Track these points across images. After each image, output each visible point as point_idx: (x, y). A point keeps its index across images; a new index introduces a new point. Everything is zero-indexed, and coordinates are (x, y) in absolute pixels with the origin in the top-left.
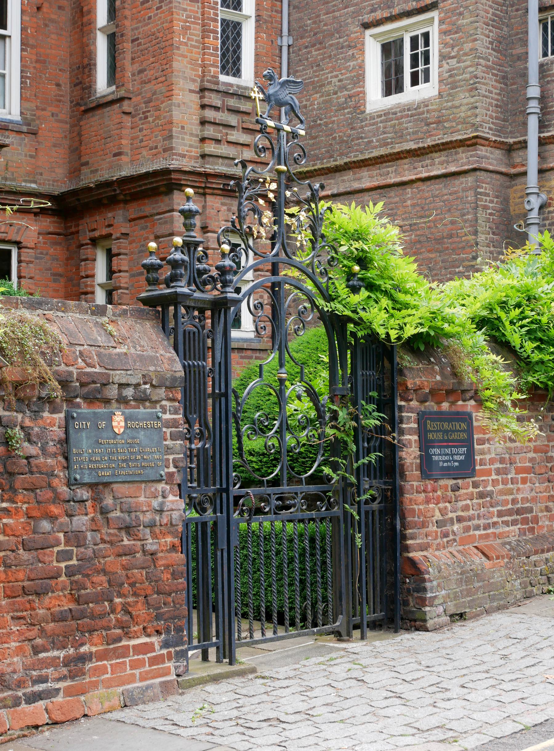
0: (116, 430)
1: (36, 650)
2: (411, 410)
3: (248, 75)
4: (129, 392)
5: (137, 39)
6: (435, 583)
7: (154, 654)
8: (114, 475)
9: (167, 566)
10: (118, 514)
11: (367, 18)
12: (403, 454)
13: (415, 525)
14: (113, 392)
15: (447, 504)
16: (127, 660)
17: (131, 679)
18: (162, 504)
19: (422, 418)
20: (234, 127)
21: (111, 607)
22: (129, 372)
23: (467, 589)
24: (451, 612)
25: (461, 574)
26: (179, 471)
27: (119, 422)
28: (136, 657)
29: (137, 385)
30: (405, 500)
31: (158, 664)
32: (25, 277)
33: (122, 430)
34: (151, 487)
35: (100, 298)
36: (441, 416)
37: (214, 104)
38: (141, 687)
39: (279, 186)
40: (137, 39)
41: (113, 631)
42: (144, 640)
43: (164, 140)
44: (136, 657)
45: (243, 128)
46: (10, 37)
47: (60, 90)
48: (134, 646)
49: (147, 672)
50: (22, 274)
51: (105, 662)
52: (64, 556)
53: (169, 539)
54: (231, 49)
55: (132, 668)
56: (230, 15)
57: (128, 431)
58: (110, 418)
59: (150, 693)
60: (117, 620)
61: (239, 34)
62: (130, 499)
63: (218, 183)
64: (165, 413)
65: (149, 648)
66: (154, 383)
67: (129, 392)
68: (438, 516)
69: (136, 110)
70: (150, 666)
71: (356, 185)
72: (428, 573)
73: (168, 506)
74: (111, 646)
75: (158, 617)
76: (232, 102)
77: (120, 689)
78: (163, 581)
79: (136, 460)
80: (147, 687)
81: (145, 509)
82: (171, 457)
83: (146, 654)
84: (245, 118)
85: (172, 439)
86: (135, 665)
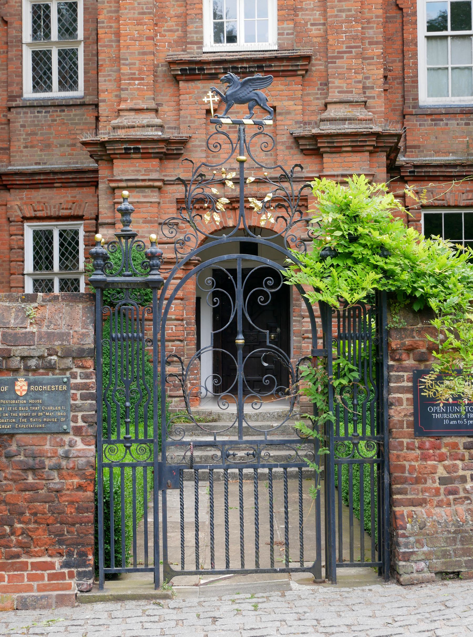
0: (18, 393)
2: (405, 369)
4: (33, 363)
6: (412, 539)
7: (54, 571)
8: (13, 428)
9: (71, 503)
10: (22, 458)
12: (392, 412)
13: (405, 481)
14: (15, 363)
15: (458, 462)
16: (25, 573)
17: (30, 588)
18: (67, 452)
21: (11, 530)
22: (32, 347)
23: (463, 549)
24: (438, 570)
25: (455, 532)
26: (90, 426)
27: (21, 386)
28: (34, 572)
29: (41, 357)
30: (391, 456)
31: (57, 580)
33: (24, 393)
34: (56, 438)
35: (29, 288)
38: (37, 597)
41: (13, 549)
42: (46, 559)
44: (34, 572)
48: (32, 563)
49: (45, 585)
51: (3, 573)
53: (76, 481)
55: (29, 580)
57: (31, 394)
58: (13, 383)
59: (44, 602)
60: (17, 541)
62: (34, 447)
64: (75, 378)
65: (51, 566)
66: (59, 354)
67: (33, 363)
68: (441, 472)
70: (48, 580)
72: (405, 528)
73: (73, 453)
74: (10, 561)
75: (60, 542)
77: (15, 596)
78: (67, 514)
79: (37, 416)
80: (42, 598)
81: (49, 455)
82: (80, 414)
83: (45, 570)
85: (82, 399)
86: (32, 578)
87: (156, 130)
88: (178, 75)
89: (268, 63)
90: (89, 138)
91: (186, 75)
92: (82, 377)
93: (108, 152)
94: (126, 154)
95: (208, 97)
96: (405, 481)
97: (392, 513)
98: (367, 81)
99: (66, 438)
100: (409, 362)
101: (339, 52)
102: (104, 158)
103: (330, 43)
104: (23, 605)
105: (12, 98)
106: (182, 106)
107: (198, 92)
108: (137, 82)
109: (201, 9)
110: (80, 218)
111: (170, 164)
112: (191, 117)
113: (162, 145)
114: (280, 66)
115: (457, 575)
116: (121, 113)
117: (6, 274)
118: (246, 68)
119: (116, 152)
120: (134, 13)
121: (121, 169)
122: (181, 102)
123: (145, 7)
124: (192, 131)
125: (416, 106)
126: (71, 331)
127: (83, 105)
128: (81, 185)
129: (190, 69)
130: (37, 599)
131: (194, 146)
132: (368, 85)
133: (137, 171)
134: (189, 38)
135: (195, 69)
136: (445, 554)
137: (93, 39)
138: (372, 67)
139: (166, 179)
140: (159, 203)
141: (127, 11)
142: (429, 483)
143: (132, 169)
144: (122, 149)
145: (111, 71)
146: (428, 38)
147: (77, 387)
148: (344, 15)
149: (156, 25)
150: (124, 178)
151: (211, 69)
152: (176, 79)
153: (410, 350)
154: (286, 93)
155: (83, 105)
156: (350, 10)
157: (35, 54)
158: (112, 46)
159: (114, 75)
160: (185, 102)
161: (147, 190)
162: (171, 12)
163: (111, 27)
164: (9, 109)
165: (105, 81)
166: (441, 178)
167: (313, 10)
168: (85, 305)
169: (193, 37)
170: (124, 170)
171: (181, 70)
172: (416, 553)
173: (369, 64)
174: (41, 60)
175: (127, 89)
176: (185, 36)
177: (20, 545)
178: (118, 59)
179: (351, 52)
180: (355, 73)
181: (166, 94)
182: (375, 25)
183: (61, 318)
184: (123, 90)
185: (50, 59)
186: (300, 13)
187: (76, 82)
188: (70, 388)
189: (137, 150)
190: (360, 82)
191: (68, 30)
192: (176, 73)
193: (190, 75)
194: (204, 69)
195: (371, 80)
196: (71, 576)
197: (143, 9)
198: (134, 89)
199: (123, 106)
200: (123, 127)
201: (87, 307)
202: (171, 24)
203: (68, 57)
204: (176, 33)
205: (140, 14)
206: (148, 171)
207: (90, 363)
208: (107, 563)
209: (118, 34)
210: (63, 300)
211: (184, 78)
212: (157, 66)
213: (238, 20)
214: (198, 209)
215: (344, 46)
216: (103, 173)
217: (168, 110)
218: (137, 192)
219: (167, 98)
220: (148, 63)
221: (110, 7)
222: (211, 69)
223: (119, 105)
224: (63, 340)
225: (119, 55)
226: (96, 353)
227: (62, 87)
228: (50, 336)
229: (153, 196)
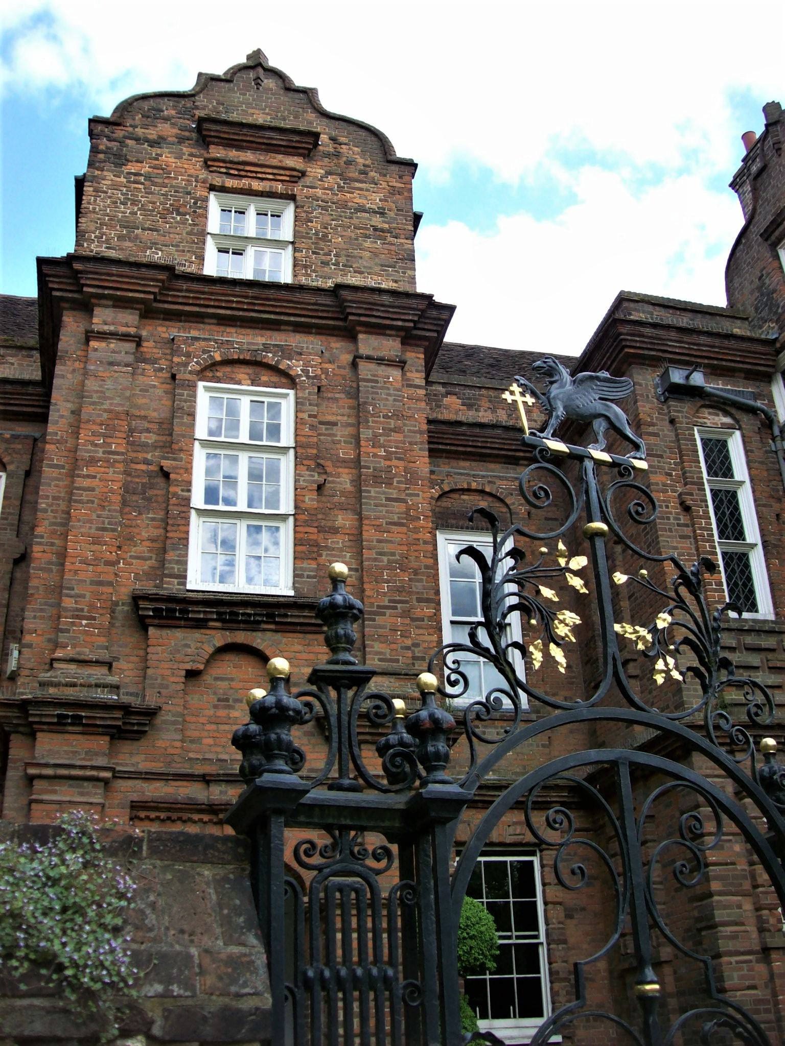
3: (765, 609)
5: (633, 594)
20: (757, 668)
32: (550, 884)
37: (728, 645)
39: (593, 560)
40: (633, 594)
43: (674, 696)
45: (769, 668)
46: (510, 624)
47: (573, 672)
50: (547, 881)
54: (740, 584)
56: (733, 546)
61: (747, 566)
69: (643, 671)
76: (749, 640)
84: (770, 656)
87: (110, 692)
88: (149, 616)
89: (282, 611)
91: (161, 617)
93: (31, 719)
94: (60, 725)
95: (512, 393)
98: (416, 650)
101: (379, 607)
102: (21, 729)
103: (367, 593)
106: (150, 663)
107: (176, 645)
108: (84, 622)
109: (187, 532)
112: (163, 678)
113: (118, 714)
114: (299, 616)
116: (56, 665)
118: (249, 615)
119: (44, 720)
120: (90, 528)
121: (47, 747)
122: (149, 657)
123: (107, 521)
124: (163, 700)
126: (194, 951)
129: (167, 610)
131: (165, 722)
132: (417, 654)
133: (75, 753)
134: (168, 568)
135: (175, 610)
138: (421, 631)
139: (118, 768)
140: (103, 806)
141: (81, 524)
143: (66, 748)
144: (53, 716)
145: (46, 604)
146: (452, 622)
148: (385, 559)
149: (119, 548)
150: (52, 762)
151: (199, 612)
152: (142, 625)
154: (304, 656)
156: (393, 554)
158: (51, 571)
160: (154, 657)
161: (86, 784)
162: (143, 534)
163: (52, 544)
165: (35, 617)
166: (480, 805)
167: (341, 550)
168: (220, 871)
169: (173, 568)
170: (52, 748)
171: (154, 610)
173: (418, 627)
175: (68, 631)
176: (163, 566)
178: (59, 589)
179: (395, 608)
180: (401, 636)
182: (424, 578)
183: (153, 905)
184: (62, 631)
186: (324, 553)
190: (408, 648)
192: (146, 613)
193: (166, 618)
194: (188, 612)
195: (421, 648)
197: (103, 523)
198: (80, 632)
199: (59, 654)
200: (57, 685)
201: (225, 879)
202: (143, 549)
204: (148, 562)
205: (98, 529)
206: (90, 753)
210: (153, 851)
211: (156, 621)
212: (116, 604)
213: (237, 553)
214: (163, 821)
215: (386, 599)
218: (71, 786)
219: (127, 650)
220: (104, 597)
221: (55, 517)
222: (199, 612)
223: (54, 651)
224: (168, 981)
225: (62, 583)
229: (96, 794)
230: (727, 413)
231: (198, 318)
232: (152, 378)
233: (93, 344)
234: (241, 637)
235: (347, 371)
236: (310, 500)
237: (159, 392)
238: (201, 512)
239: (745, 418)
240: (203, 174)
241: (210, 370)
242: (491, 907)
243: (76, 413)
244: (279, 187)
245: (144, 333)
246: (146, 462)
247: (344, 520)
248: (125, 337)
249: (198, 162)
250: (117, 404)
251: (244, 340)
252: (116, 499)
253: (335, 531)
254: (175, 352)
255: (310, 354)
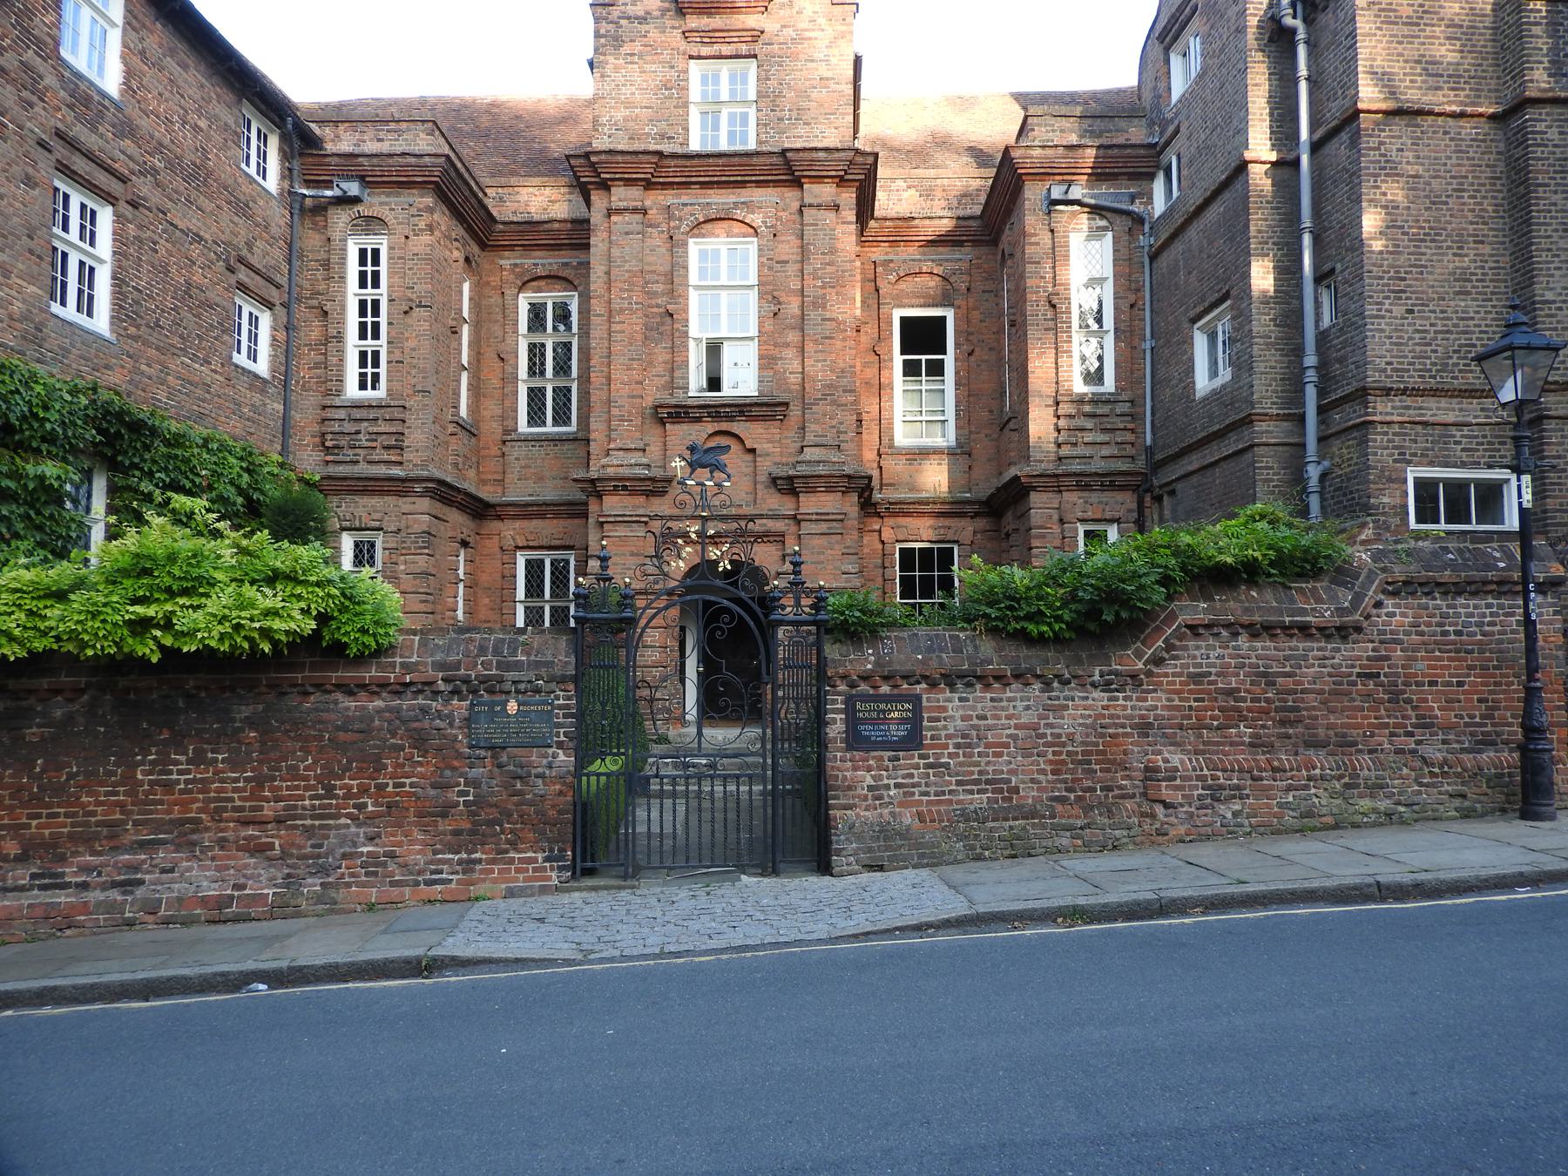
1: (435, 853)
4: (522, 687)
11: (1192, 314)
13: (837, 788)
17: (516, 880)
19: (850, 701)
27: (512, 707)
36: (866, 698)
52: (462, 793)
63: (1067, 481)
65: (535, 860)
67: (522, 687)
68: (869, 781)
71: (1190, 468)
86: (518, 871)
90: (581, 474)
92: (563, 698)
96: (837, 788)
97: (827, 815)
99: (550, 751)
100: (842, 687)
104: (510, 894)
105: (506, 432)
110: (570, 548)
111: (656, 501)
115: (881, 868)
117: (498, 601)
125: (891, 446)
127: (575, 440)
128: (572, 516)
130: (522, 889)
136: (870, 850)
137: (585, 379)
142: (859, 791)
147: (560, 707)
153: (844, 677)
155: (575, 440)
157: (531, 390)
159: (605, 416)
164: (504, 442)
170: (614, 504)
172: (846, 849)
174: (536, 396)
177: (508, 842)
181: (653, 436)
185: (544, 395)
187: (569, 418)
188: (554, 708)
189: (625, 488)
191: (562, 368)
196: (552, 869)
202: (660, 369)
203: (563, 394)
206: (635, 507)
207: (572, 687)
208: (584, 860)
209: (609, 379)
216: (593, 507)
217: (655, 450)
226: (576, 679)
227: (556, 422)
228: (538, 664)
230: (1103, 217)
231: (686, 185)
232: (657, 239)
233: (614, 218)
234: (724, 426)
235: (796, 217)
236: (769, 326)
237: (663, 250)
238: (697, 287)
239: (1118, 220)
240: (683, 45)
241: (698, 228)
242: (459, 662)
243: (608, 273)
244: (744, 49)
245: (648, 203)
246: (658, 306)
247: (793, 337)
248: (635, 210)
249: (677, 34)
250: (633, 265)
251: (720, 199)
252: (639, 337)
253: (787, 345)
254: (670, 217)
255: (766, 204)
